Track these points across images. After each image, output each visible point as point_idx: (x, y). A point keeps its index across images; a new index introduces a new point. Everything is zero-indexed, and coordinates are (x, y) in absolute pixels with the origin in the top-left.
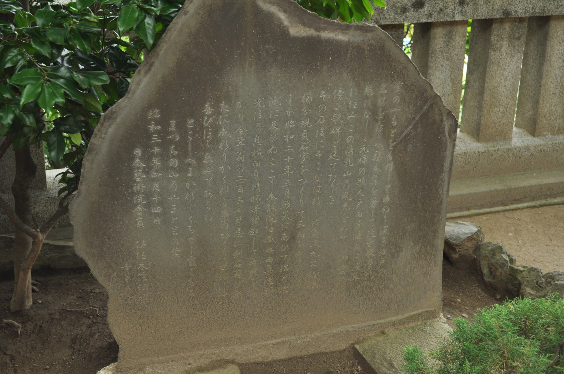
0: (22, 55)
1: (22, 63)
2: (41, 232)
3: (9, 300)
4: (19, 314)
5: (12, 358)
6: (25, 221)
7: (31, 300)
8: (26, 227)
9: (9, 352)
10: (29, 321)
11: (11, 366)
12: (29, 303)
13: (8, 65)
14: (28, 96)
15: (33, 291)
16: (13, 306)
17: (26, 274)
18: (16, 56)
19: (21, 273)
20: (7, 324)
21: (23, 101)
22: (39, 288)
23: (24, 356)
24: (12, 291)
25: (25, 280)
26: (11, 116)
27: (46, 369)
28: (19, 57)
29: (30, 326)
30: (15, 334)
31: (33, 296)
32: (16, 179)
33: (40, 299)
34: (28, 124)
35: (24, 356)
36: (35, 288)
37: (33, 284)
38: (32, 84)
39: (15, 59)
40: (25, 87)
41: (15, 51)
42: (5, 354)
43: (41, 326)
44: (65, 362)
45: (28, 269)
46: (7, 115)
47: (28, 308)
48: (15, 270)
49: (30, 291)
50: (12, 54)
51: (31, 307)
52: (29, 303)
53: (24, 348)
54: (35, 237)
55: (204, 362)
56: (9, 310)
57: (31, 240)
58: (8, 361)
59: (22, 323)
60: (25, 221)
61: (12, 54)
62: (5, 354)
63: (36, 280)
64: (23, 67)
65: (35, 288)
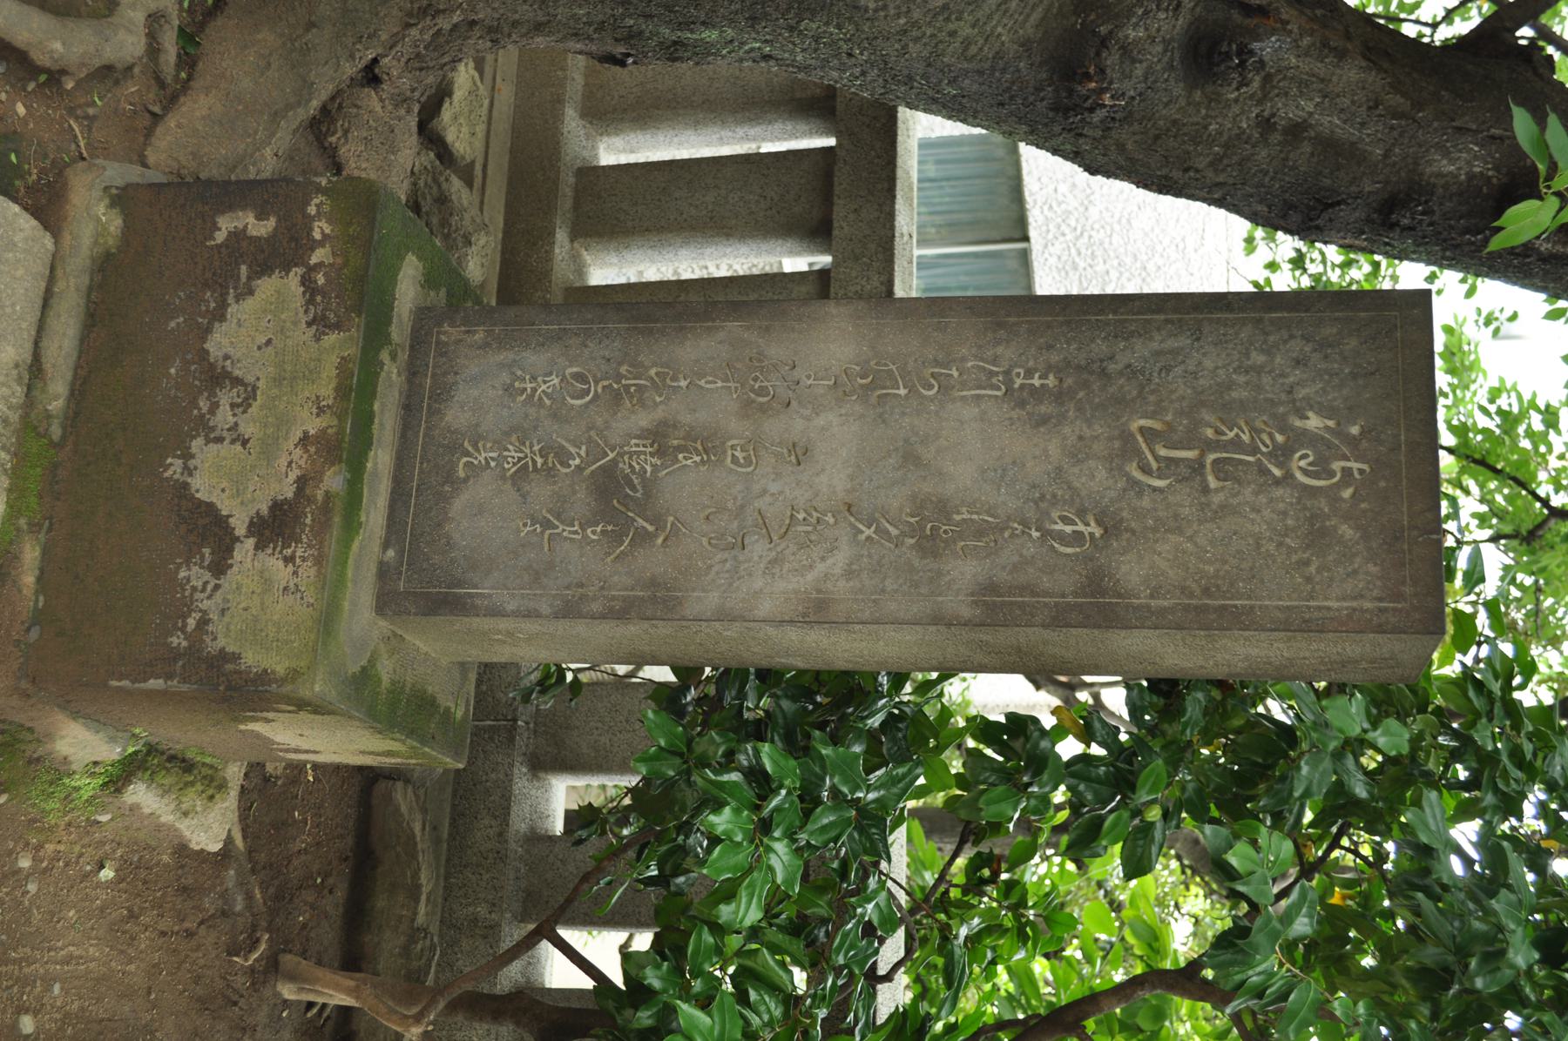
0: (770, 1024)
1: (755, 1021)
2: (426, 1032)
3: (304, 954)
4: (272, 967)
5: (190, 934)
6: (453, 1007)
7: (292, 997)
8: (441, 1005)
9: (202, 930)
10: (253, 984)
11: (176, 928)
12: (288, 992)
13: (753, 995)
14: (691, 1017)
15: (310, 1005)
16: (288, 960)
17: (349, 991)
18: (769, 1011)
19: (352, 983)
20: (258, 940)
21: (684, 1007)
22: (311, 1021)
23: (187, 956)
24: (319, 963)
25: (338, 987)
26: (656, 984)
27: (149, 993)
28: (766, 1017)
29: (242, 982)
30: (233, 950)
31: (299, 1002)
32: (539, 1002)
33: (289, 1015)
34: (639, 1014)
35: (187, 956)
36: (315, 1010)
37: (324, 1006)
38: (712, 1028)
39: (763, 1008)
40: (710, 1015)
41: (778, 1012)
42: (202, 923)
43: (235, 1003)
44: (152, 1033)
45: (357, 998)
46: (661, 978)
47: (279, 987)
48: (358, 975)
49: (311, 998)
50: (772, 1006)
51: (278, 995)
52: (288, 992)
53: (202, 962)
54: (418, 1019)
55: (59, 286)
56: (284, 951)
57: (414, 1010)
58: (187, 925)
59: (252, 970)
60: (453, 1007)
61: (772, 1006)
62: (202, 923)
63: (329, 1017)
64: (747, 1022)
65: (315, 1010)
